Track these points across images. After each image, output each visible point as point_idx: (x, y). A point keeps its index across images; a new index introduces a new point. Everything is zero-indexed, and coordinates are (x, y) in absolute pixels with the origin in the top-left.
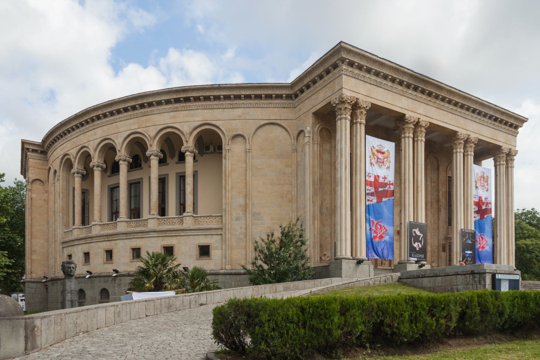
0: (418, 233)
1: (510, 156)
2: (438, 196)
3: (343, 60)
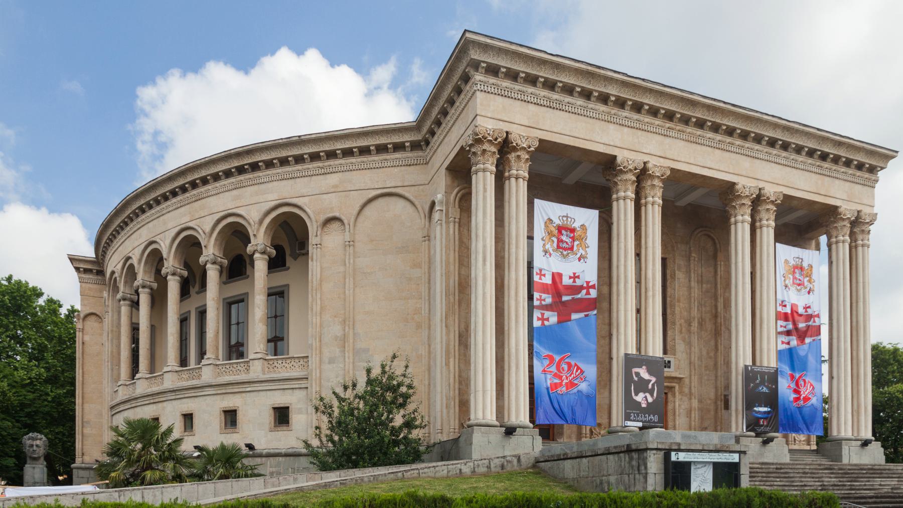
0: (645, 375)
1: (859, 225)
2: (716, 307)
3: (476, 65)
